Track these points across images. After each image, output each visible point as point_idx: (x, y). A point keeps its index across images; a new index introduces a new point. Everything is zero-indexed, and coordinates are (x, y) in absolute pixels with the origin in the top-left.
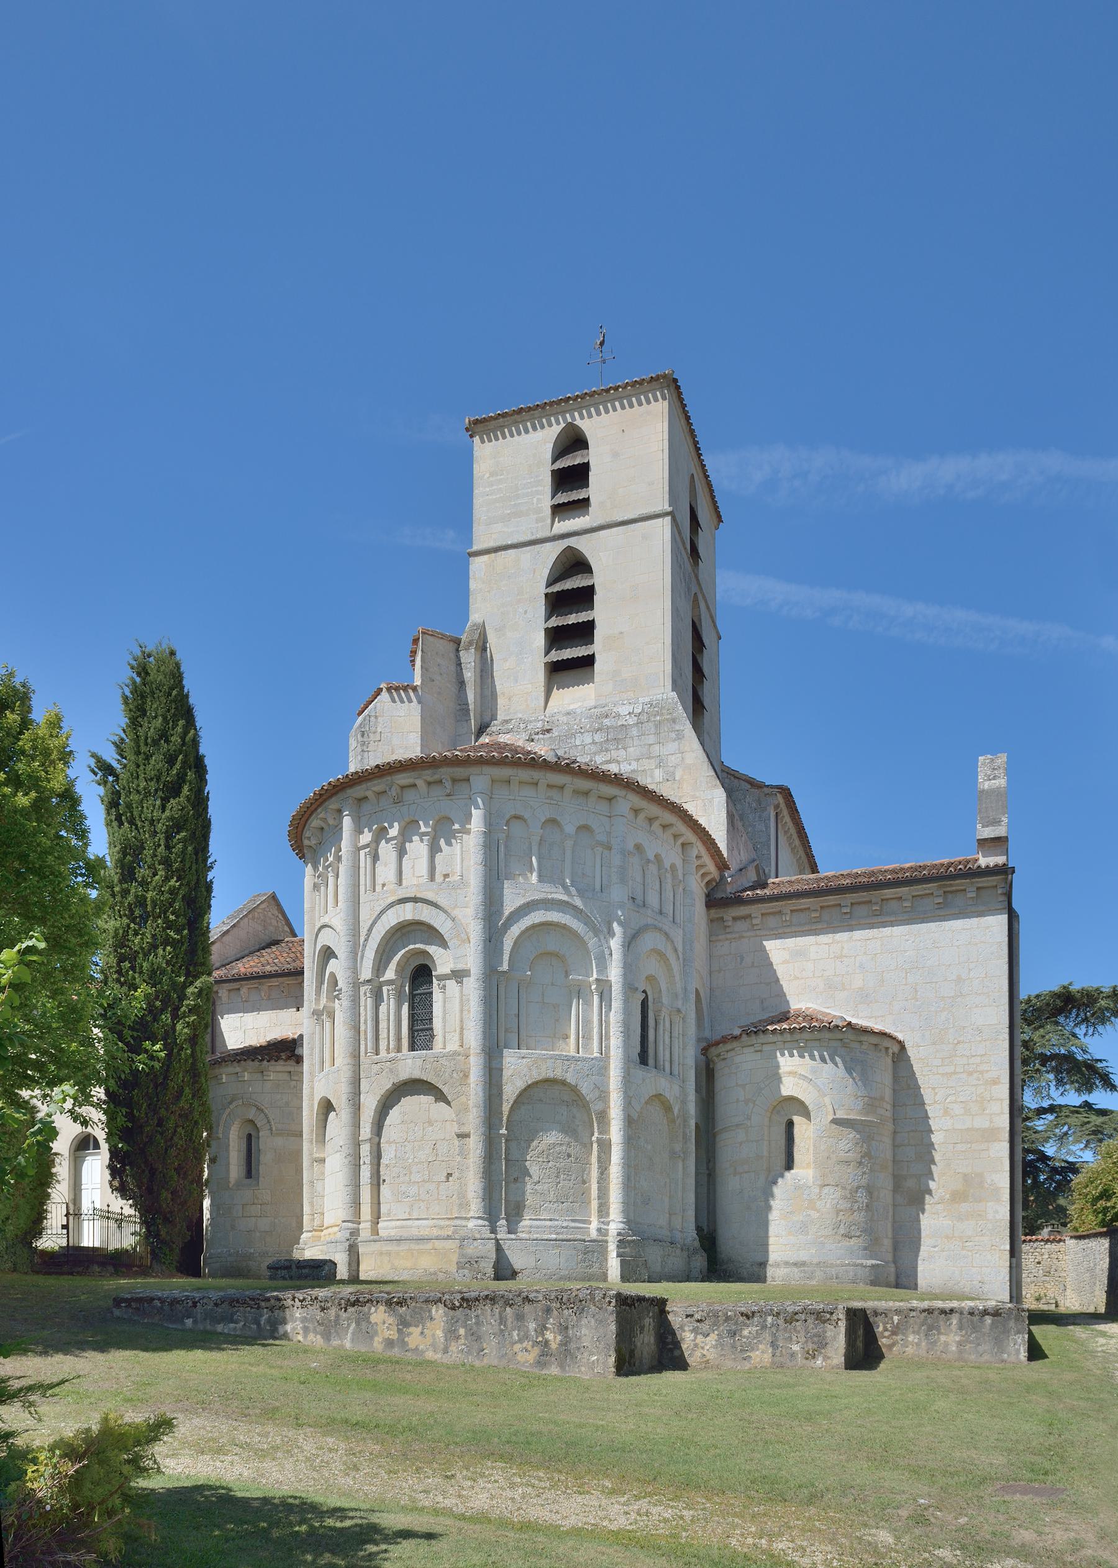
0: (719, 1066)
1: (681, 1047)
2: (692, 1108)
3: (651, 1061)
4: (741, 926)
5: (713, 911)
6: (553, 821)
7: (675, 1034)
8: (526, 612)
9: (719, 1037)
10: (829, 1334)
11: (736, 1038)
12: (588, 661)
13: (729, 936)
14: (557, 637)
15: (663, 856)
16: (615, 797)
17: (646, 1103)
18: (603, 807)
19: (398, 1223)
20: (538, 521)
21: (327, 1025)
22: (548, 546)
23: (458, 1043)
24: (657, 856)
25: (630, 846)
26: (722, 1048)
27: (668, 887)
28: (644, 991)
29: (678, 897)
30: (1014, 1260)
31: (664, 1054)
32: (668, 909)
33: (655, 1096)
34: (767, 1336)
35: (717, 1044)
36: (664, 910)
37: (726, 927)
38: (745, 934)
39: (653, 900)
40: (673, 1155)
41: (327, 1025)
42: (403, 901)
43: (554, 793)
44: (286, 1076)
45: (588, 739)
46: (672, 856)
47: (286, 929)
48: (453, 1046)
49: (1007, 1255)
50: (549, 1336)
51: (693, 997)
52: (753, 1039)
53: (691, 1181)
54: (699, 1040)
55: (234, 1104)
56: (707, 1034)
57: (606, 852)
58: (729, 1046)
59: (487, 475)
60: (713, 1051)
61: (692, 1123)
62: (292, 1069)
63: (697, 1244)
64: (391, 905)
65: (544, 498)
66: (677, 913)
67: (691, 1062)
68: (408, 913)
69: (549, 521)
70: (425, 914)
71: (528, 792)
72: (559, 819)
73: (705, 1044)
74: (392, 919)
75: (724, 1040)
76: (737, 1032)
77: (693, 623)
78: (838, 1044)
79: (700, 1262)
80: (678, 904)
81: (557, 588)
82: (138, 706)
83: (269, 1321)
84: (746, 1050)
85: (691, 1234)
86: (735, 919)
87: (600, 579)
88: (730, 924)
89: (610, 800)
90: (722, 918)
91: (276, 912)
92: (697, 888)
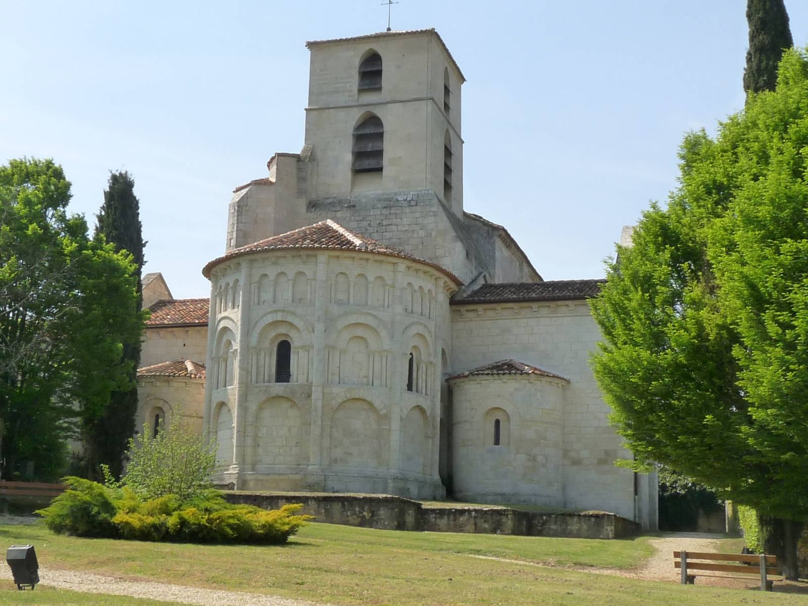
0: (455, 389)
1: (432, 380)
2: (438, 411)
3: (414, 388)
4: (471, 315)
5: (453, 306)
6: (362, 275)
7: (429, 373)
8: (340, 143)
9: (456, 375)
10: (503, 520)
11: (466, 376)
12: (380, 170)
13: (463, 319)
14: (359, 155)
15: (424, 286)
16: (397, 263)
17: (411, 410)
18: (390, 267)
19: (267, 466)
20: (349, 96)
21: (223, 365)
22: (355, 109)
23: (306, 379)
24: (420, 287)
25: (405, 285)
26: (457, 381)
27: (426, 301)
28: (411, 354)
29: (432, 306)
30: (637, 497)
31: (422, 384)
32: (426, 311)
33: (417, 406)
34: (472, 521)
35: (455, 378)
36: (424, 313)
37: (462, 315)
38: (473, 319)
39: (417, 309)
40: (427, 437)
41: (223, 365)
42: (276, 311)
43: (362, 262)
44: (184, 385)
45: (378, 212)
46: (428, 285)
47: (167, 293)
48: (302, 379)
49: (633, 493)
50: (365, 513)
51: (440, 355)
52: (476, 377)
53: (437, 450)
54: (444, 374)
55: (150, 398)
56: (449, 370)
57: (391, 289)
58: (462, 380)
59: (318, 71)
60: (452, 382)
61: (438, 420)
62: (187, 381)
63: (440, 481)
64: (269, 313)
65: (354, 82)
66: (431, 312)
67: (438, 387)
68: (279, 317)
69: (356, 97)
70: (289, 319)
71: (349, 262)
72: (365, 274)
73: (447, 377)
74: (269, 319)
75: (458, 377)
76: (467, 373)
77: (446, 147)
78: (528, 381)
79: (442, 491)
80: (432, 308)
81: (361, 132)
82: (110, 196)
83: (733, 392)
84: (471, 382)
85: (437, 477)
86: (467, 311)
87: (387, 127)
88: (464, 313)
89: (394, 264)
90: (460, 310)
91: (161, 284)
92: (443, 298)
